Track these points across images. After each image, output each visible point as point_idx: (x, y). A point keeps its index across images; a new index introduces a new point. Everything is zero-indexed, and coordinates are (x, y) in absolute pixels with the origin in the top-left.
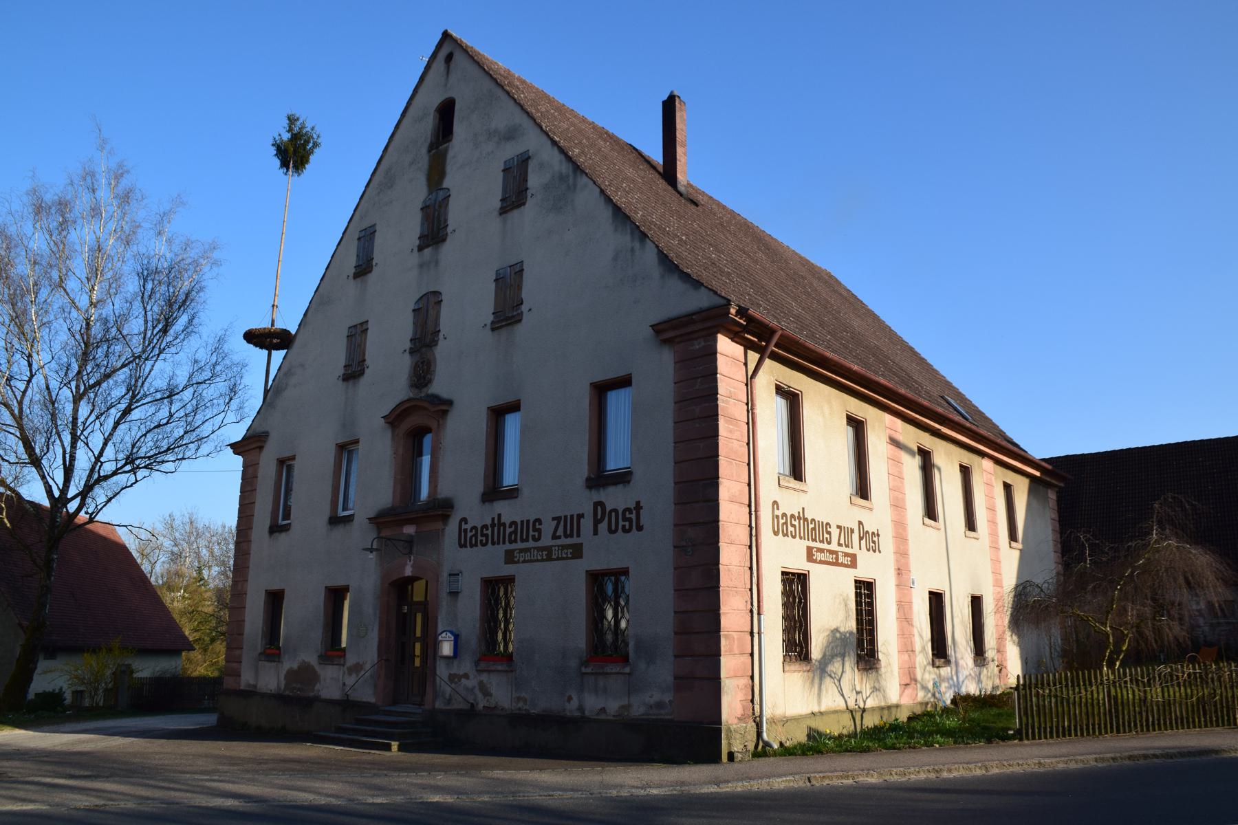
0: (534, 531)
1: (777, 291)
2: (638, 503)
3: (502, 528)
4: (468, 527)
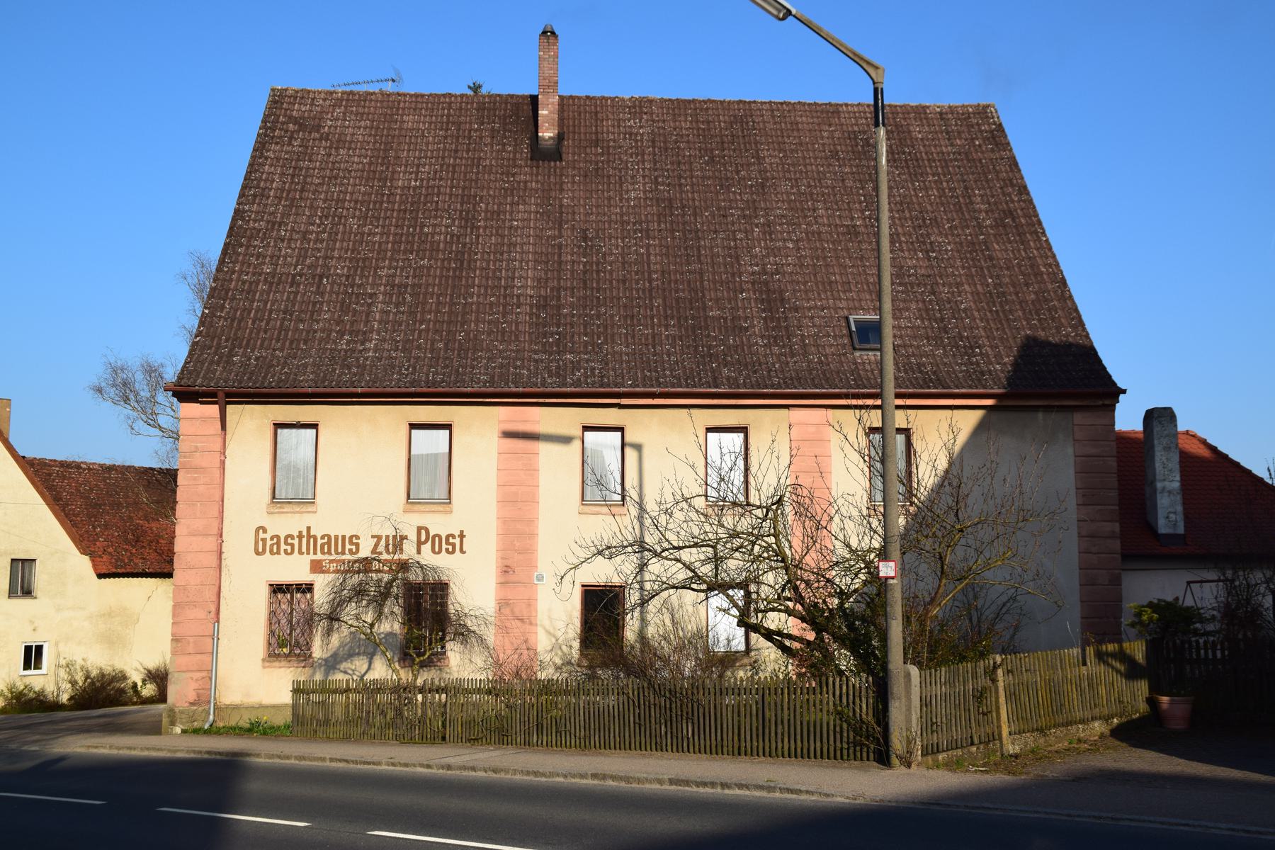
0: (446, 544)
1: (417, 732)
2: (462, 532)
3: (312, 540)
4: (268, 536)
